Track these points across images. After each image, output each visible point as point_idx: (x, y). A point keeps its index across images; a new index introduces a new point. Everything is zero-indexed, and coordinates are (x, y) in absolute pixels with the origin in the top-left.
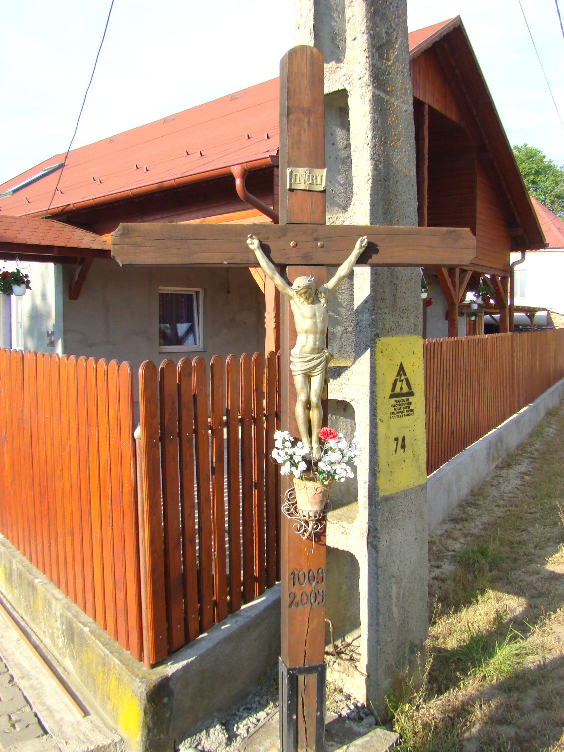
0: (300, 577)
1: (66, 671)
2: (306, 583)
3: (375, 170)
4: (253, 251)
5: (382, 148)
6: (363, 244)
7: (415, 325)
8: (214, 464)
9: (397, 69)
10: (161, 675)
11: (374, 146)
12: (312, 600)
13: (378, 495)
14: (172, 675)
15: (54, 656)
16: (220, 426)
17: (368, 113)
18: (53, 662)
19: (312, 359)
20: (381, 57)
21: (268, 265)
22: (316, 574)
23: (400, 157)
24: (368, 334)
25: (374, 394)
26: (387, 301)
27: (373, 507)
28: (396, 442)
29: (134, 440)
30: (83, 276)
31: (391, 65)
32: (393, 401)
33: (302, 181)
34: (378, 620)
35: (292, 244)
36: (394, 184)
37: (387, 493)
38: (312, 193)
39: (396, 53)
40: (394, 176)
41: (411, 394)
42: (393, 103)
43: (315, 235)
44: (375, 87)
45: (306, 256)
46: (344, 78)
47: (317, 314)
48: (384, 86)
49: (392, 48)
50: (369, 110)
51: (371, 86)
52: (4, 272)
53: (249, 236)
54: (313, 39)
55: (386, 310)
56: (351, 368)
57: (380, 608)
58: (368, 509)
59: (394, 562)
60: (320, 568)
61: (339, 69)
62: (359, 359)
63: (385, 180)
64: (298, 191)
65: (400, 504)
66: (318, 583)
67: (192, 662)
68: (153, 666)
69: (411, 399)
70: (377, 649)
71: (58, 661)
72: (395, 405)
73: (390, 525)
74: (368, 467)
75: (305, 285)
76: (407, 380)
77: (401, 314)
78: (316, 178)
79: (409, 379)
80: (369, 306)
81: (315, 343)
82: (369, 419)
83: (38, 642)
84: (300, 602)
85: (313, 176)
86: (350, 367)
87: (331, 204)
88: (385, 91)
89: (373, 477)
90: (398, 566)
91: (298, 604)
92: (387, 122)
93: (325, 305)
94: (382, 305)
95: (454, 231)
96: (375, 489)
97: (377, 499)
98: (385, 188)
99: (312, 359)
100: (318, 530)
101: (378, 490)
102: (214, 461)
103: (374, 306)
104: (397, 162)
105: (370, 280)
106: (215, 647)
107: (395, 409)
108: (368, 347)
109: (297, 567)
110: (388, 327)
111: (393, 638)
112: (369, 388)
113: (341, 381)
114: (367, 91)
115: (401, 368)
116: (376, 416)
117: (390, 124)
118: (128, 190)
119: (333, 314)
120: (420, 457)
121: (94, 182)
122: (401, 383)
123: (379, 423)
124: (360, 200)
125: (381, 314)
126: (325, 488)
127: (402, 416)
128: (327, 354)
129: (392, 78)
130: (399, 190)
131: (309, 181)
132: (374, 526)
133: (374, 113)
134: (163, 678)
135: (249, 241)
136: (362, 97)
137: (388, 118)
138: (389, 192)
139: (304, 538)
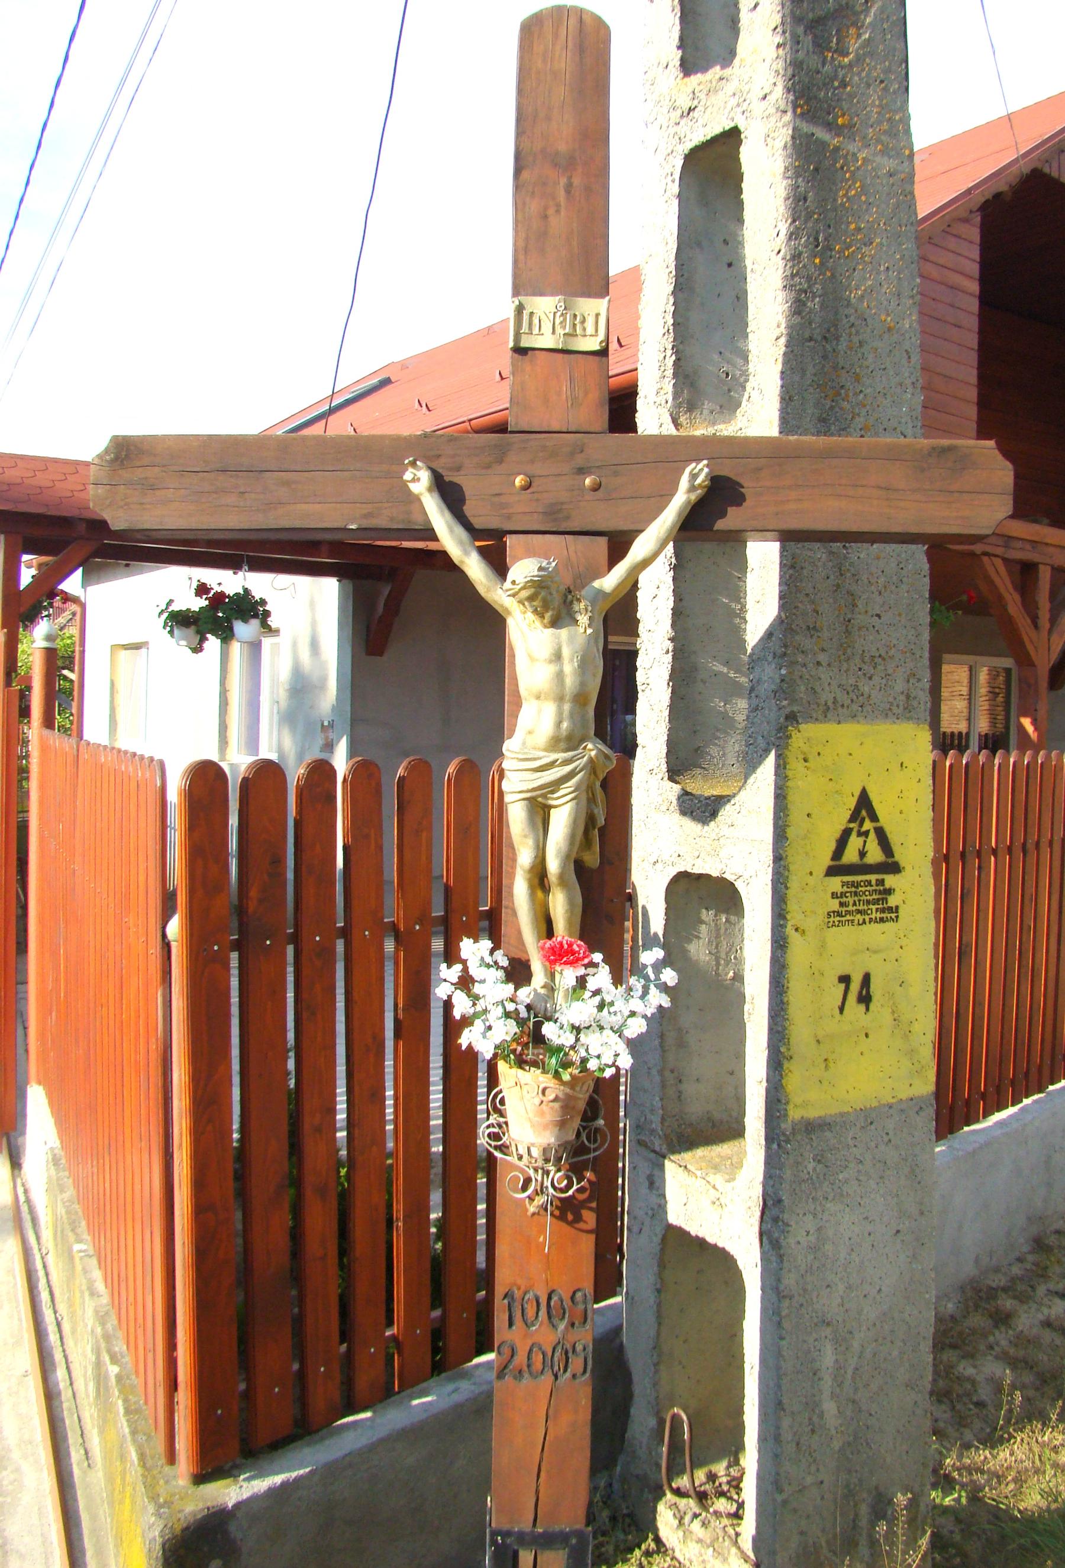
0: (526, 1306)
1: (87, 1458)
2: (542, 1321)
3: (795, 313)
4: (417, 499)
5: (817, 261)
6: (699, 481)
7: (908, 697)
8: (400, 1012)
9: (868, 75)
10: (209, 1504)
11: (796, 257)
12: (556, 1368)
13: (786, 1115)
14: (238, 1505)
15: (80, 1421)
16: (421, 925)
17: (779, 177)
18: (70, 1434)
19: (552, 765)
20: (820, 45)
21: (451, 531)
22: (567, 1303)
23: (870, 283)
24: (772, 714)
25: (782, 863)
26: (826, 634)
27: (775, 1146)
28: (842, 986)
29: (166, 946)
30: (393, 606)
31: (850, 65)
32: (836, 883)
33: (547, 327)
34: (778, 1428)
35: (519, 481)
36: (851, 349)
37: (812, 1114)
38: (572, 356)
39: (867, 36)
40: (853, 330)
41: (894, 868)
42: (854, 154)
43: (579, 460)
44: (802, 115)
45: (553, 511)
46: (733, 102)
47: (566, 652)
48: (829, 114)
49: (854, 24)
50: (782, 169)
51: (789, 114)
52: (217, 593)
53: (406, 462)
54: (677, 22)
55: (822, 657)
56: (737, 798)
57: (785, 1400)
58: (763, 1148)
59: (828, 1286)
60: (579, 1290)
61: (724, 81)
62: (754, 775)
63: (825, 338)
64: (537, 352)
65: (851, 1143)
66: (573, 1325)
67: (297, 1479)
68: (200, 1479)
69: (890, 880)
70: (774, 1500)
71: (82, 1435)
72: (843, 895)
73: (820, 1193)
74: (766, 1045)
75: (529, 579)
76: (881, 834)
77: (865, 667)
78: (583, 321)
79: (888, 830)
80: (775, 645)
81: (559, 723)
82: (769, 926)
83: (63, 1384)
84: (525, 1368)
85: (575, 316)
86: (734, 795)
87: (721, 407)
88: (829, 126)
89: (776, 1069)
90: (842, 1298)
91: (520, 1372)
92: (835, 200)
93: (589, 631)
94: (807, 643)
95: (950, 449)
96: (779, 1101)
97: (783, 1126)
98: (825, 357)
99: (552, 765)
100: (570, 1192)
101: (787, 1103)
102: (401, 1005)
103: (785, 646)
104: (862, 296)
105: (778, 582)
106: (372, 1448)
107: (841, 904)
108: (771, 746)
109: (519, 1281)
110: (826, 697)
111: (820, 1477)
112: (771, 847)
113: (717, 830)
114: (780, 124)
115: (864, 805)
116: (785, 918)
117: (843, 205)
118: (464, 422)
119: (725, 670)
120: (916, 1027)
121: (428, 412)
122: (861, 840)
123: (794, 937)
124: (760, 387)
125: (805, 665)
126: (568, 1090)
127: (864, 922)
128: (593, 753)
129: (851, 96)
130: (866, 363)
131: (565, 328)
132: (774, 1193)
133: (797, 177)
134: (212, 1510)
135: (408, 476)
136: (769, 139)
137: (838, 191)
138: (835, 368)
139: (532, 1209)
